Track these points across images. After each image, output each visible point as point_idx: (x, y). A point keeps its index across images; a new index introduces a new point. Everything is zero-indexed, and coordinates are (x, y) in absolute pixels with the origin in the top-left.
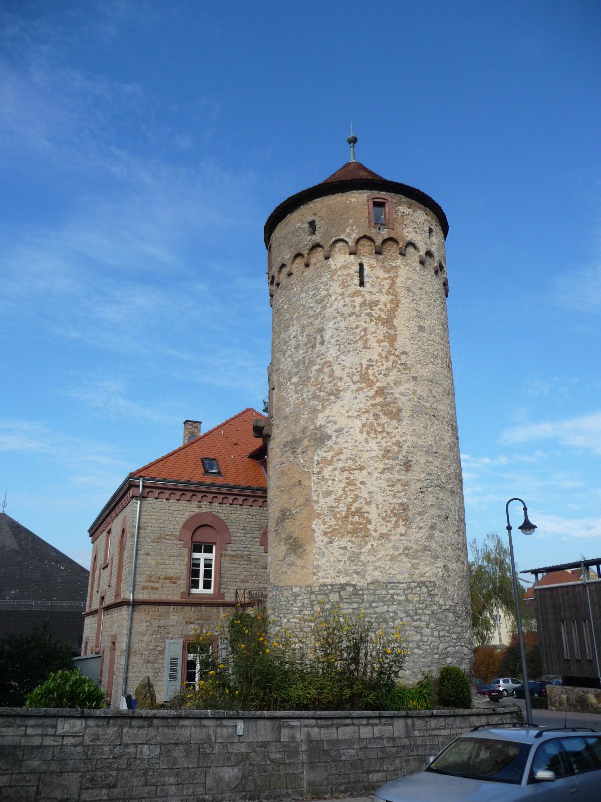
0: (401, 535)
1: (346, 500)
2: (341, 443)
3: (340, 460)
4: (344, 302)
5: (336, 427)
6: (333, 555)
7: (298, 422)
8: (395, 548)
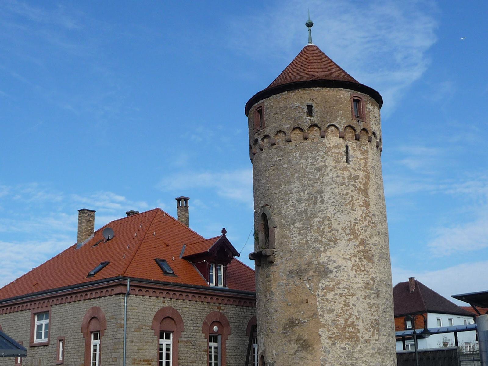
0: (376, 340)
1: (344, 316)
3: (339, 288)
5: (336, 265)
7: (303, 257)
8: (373, 349)
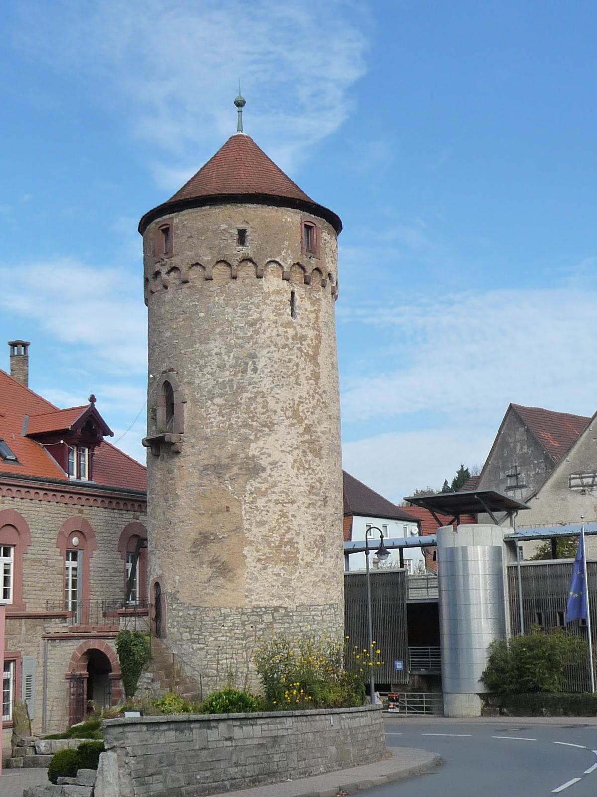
0: (321, 564)
2: (275, 477)
3: (274, 492)
4: (278, 331)
5: (270, 460)
7: (224, 447)
8: (317, 576)
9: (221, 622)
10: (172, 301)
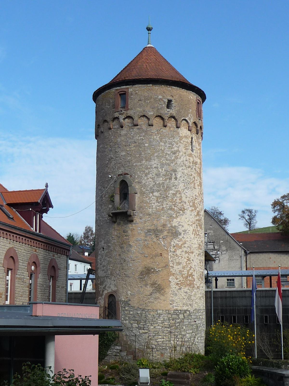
3: (185, 247)
4: (186, 158)
5: (183, 229)
6: (181, 296)
9: (158, 318)
10: (126, 135)
